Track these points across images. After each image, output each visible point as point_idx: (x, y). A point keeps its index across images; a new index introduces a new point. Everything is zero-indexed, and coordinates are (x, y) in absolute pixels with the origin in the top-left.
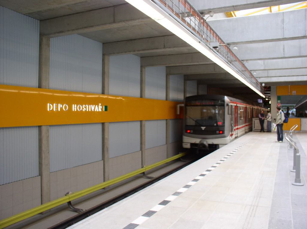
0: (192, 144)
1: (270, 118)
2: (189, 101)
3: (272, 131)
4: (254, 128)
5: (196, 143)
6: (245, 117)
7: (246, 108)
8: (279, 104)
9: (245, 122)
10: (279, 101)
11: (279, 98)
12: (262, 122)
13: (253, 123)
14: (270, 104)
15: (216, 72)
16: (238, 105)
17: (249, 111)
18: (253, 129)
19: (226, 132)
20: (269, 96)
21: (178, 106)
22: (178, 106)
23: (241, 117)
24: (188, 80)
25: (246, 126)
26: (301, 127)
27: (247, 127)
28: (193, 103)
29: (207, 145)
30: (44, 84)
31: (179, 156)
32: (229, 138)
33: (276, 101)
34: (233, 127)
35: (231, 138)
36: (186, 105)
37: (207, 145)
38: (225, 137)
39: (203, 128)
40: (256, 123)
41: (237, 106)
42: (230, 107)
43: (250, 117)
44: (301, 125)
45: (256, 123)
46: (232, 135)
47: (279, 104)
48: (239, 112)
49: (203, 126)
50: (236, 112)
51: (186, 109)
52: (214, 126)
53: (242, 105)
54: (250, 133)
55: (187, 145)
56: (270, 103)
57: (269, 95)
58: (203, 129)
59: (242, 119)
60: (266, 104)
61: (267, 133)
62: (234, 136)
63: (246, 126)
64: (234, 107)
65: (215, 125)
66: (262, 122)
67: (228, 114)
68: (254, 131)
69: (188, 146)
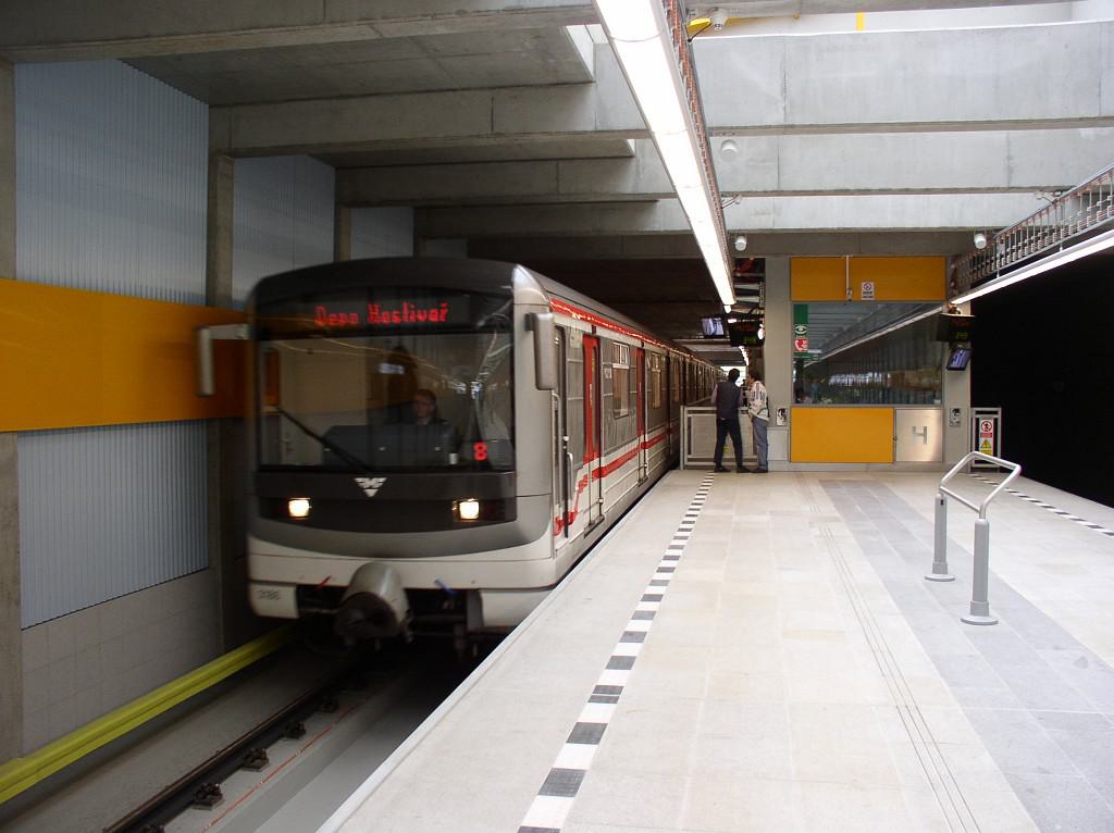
0: (305, 593)
1: (758, 402)
2: (284, 301)
3: (770, 467)
4: (689, 453)
5: (330, 583)
6: (640, 402)
7: (642, 351)
8: (800, 344)
9: (641, 430)
10: (801, 328)
11: (800, 313)
12: (728, 426)
13: (684, 425)
14: (761, 343)
15: (499, 135)
16: (600, 332)
17: (656, 369)
18: (684, 457)
19: (527, 512)
20: (756, 306)
21: (206, 335)
22: (206, 335)
23: (617, 403)
24: (235, 154)
25: (644, 446)
26: (895, 446)
27: (657, 449)
28: (324, 315)
29: (399, 606)
30: (241, 168)
31: (247, 657)
32: (543, 552)
33: (788, 332)
34: (572, 467)
35: (561, 542)
36: (263, 333)
37: (399, 606)
38: (519, 540)
39: (371, 485)
40: (699, 425)
41: (598, 339)
42: (549, 340)
43: (657, 403)
44: (895, 439)
45: (699, 425)
46: (567, 520)
47: (800, 344)
48: (606, 373)
49: (371, 472)
50: (592, 376)
51: (273, 359)
52: (451, 468)
53: (621, 339)
54: (671, 477)
55: (274, 596)
56: (760, 335)
57: (754, 299)
58: (371, 493)
59: (624, 411)
60: (744, 332)
61: (755, 475)
62: (577, 528)
63: (644, 446)
64: (576, 342)
65: (453, 459)
66: (728, 426)
67: (539, 386)
68: (686, 467)
69: (284, 605)
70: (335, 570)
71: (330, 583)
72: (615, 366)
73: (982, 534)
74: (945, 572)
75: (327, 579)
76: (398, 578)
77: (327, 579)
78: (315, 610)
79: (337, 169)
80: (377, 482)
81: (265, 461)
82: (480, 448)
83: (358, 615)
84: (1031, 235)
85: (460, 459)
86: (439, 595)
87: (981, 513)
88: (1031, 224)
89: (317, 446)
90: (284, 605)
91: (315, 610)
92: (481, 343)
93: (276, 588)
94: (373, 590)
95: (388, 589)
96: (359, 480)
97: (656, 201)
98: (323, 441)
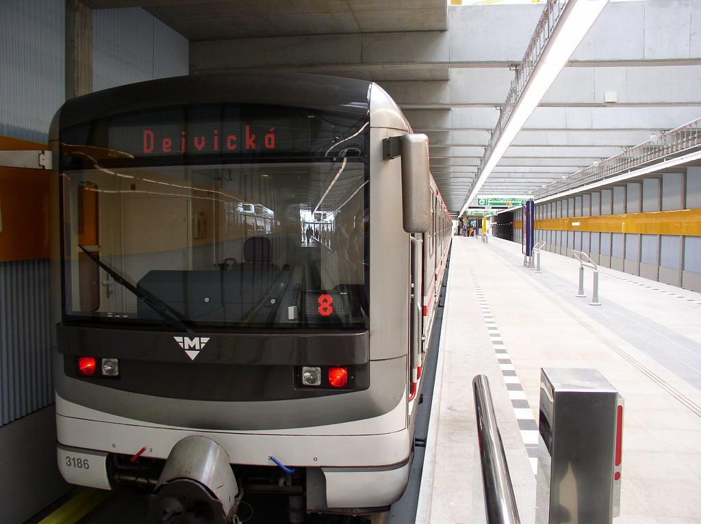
0: (116, 462)
29: (225, 491)
37: (225, 491)
38: (371, 411)
39: (193, 346)
49: (193, 329)
69: (96, 475)
70: (151, 439)
71: (144, 454)
72: (345, 159)
73: (596, 275)
74: (597, 302)
75: (143, 450)
76: (226, 453)
77: (143, 450)
78: (133, 479)
79: (191, 41)
80: (200, 342)
81: (75, 307)
82: (325, 301)
83: (175, 505)
84: (688, 136)
85: (301, 313)
86: (273, 472)
87: (596, 268)
88: (695, 127)
89: (133, 298)
90: (96, 475)
91: (133, 479)
92: (122, 273)
93: (83, 456)
94: (193, 475)
95: (211, 471)
96: (179, 339)
97: (449, 109)
98: (138, 291)
